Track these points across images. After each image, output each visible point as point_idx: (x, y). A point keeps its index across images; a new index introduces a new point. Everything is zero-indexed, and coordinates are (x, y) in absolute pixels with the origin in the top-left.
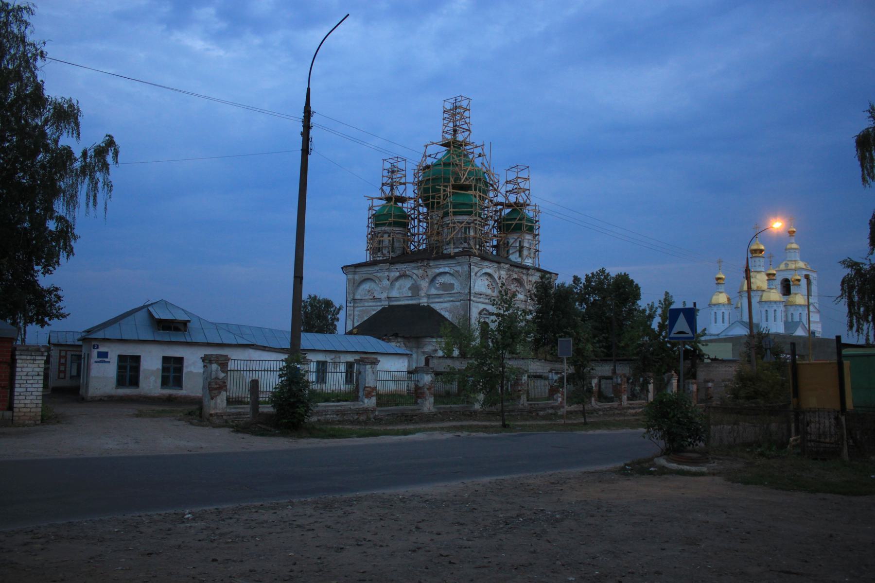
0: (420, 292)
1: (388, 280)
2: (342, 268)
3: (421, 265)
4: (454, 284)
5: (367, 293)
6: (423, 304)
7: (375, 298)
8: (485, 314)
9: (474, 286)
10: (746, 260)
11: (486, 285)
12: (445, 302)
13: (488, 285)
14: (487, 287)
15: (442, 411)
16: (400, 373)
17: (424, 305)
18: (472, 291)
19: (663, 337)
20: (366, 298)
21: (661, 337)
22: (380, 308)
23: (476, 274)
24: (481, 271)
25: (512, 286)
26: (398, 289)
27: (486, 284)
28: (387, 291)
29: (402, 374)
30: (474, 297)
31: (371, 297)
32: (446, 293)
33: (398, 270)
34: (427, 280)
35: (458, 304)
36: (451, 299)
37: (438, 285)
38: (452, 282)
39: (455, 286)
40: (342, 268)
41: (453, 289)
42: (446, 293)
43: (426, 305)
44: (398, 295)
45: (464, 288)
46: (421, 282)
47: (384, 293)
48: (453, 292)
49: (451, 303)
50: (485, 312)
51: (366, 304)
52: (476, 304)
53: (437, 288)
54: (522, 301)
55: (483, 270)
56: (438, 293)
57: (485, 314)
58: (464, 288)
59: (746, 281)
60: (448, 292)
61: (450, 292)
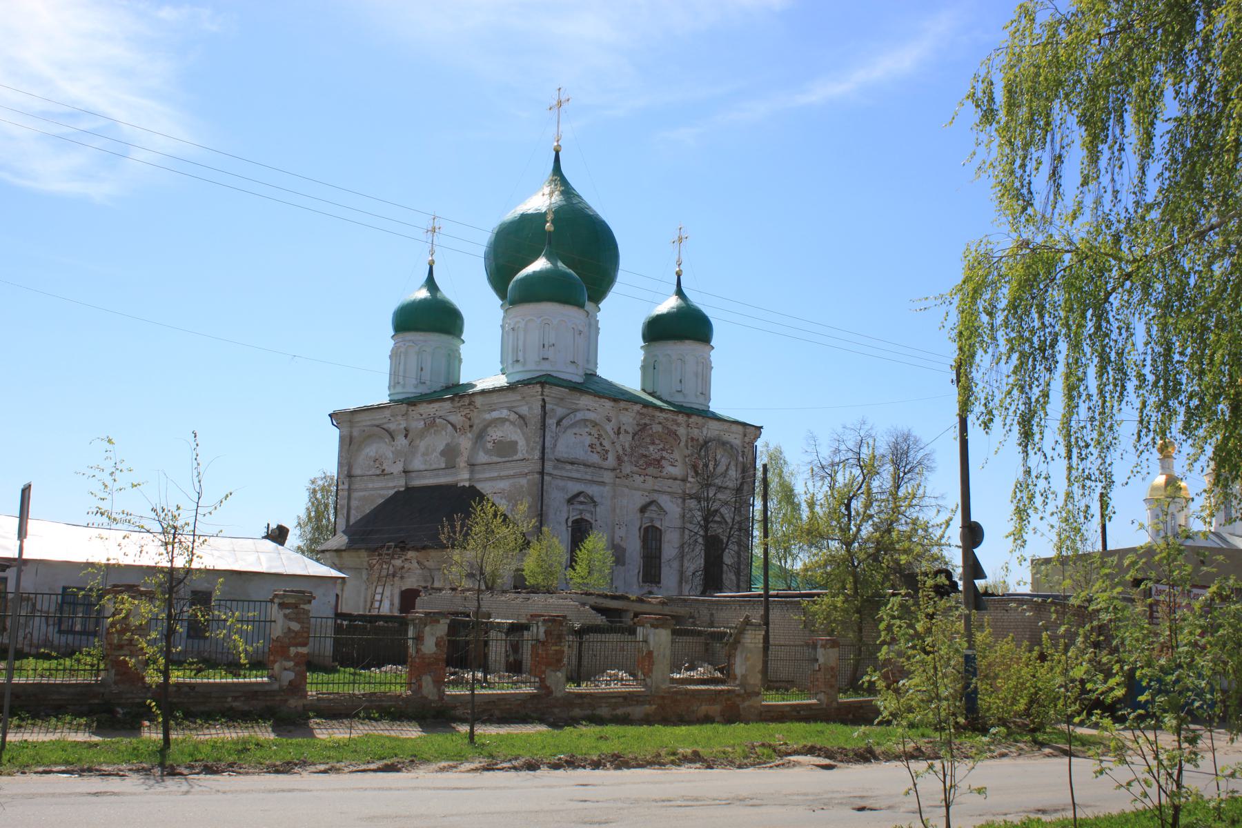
0: (458, 460)
1: (406, 436)
2: (330, 415)
3: (460, 404)
4: (516, 443)
5: (372, 463)
6: (462, 484)
7: (385, 472)
8: (582, 503)
9: (555, 445)
10: (354, 774)
11: (587, 444)
12: (501, 478)
13: (591, 446)
14: (590, 449)
15: (1155, 416)
16: (319, 620)
17: (464, 486)
18: (549, 454)
19: (914, 605)
20: (370, 473)
21: (913, 608)
22: (392, 492)
23: (558, 423)
24: (572, 416)
25: (651, 448)
26: (424, 455)
27: (588, 442)
28: (402, 460)
29: (318, 623)
30: (555, 467)
31: (378, 472)
32: (504, 459)
33: (424, 416)
34: (469, 435)
35: (523, 481)
36: (512, 472)
37: (489, 446)
38: (513, 439)
39: (519, 447)
40: (330, 415)
41: (516, 452)
42: (504, 459)
43: (467, 484)
44: (422, 467)
45: (532, 449)
46: (461, 439)
47: (398, 462)
48: (515, 458)
49: (511, 481)
50: (582, 499)
51: (371, 486)
52: (561, 483)
53: (487, 452)
54: (675, 479)
55: (577, 414)
56: (490, 460)
57: (582, 503)
58: (532, 449)
59: (134, 768)
60: (507, 459)
61: (510, 459)
